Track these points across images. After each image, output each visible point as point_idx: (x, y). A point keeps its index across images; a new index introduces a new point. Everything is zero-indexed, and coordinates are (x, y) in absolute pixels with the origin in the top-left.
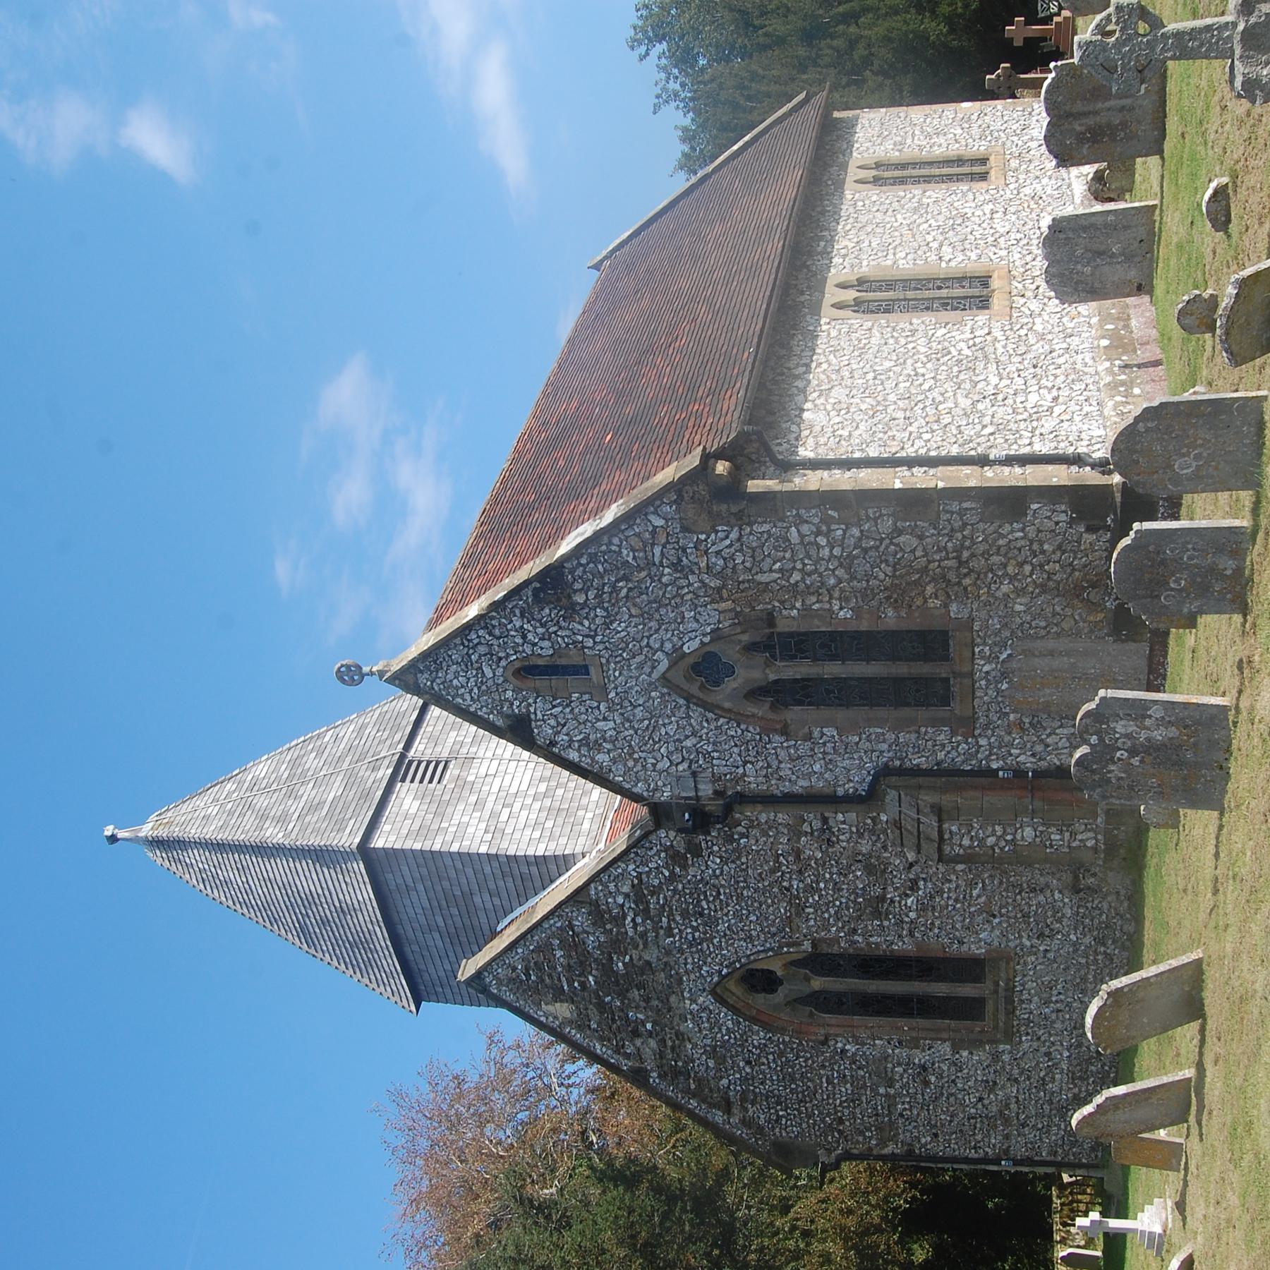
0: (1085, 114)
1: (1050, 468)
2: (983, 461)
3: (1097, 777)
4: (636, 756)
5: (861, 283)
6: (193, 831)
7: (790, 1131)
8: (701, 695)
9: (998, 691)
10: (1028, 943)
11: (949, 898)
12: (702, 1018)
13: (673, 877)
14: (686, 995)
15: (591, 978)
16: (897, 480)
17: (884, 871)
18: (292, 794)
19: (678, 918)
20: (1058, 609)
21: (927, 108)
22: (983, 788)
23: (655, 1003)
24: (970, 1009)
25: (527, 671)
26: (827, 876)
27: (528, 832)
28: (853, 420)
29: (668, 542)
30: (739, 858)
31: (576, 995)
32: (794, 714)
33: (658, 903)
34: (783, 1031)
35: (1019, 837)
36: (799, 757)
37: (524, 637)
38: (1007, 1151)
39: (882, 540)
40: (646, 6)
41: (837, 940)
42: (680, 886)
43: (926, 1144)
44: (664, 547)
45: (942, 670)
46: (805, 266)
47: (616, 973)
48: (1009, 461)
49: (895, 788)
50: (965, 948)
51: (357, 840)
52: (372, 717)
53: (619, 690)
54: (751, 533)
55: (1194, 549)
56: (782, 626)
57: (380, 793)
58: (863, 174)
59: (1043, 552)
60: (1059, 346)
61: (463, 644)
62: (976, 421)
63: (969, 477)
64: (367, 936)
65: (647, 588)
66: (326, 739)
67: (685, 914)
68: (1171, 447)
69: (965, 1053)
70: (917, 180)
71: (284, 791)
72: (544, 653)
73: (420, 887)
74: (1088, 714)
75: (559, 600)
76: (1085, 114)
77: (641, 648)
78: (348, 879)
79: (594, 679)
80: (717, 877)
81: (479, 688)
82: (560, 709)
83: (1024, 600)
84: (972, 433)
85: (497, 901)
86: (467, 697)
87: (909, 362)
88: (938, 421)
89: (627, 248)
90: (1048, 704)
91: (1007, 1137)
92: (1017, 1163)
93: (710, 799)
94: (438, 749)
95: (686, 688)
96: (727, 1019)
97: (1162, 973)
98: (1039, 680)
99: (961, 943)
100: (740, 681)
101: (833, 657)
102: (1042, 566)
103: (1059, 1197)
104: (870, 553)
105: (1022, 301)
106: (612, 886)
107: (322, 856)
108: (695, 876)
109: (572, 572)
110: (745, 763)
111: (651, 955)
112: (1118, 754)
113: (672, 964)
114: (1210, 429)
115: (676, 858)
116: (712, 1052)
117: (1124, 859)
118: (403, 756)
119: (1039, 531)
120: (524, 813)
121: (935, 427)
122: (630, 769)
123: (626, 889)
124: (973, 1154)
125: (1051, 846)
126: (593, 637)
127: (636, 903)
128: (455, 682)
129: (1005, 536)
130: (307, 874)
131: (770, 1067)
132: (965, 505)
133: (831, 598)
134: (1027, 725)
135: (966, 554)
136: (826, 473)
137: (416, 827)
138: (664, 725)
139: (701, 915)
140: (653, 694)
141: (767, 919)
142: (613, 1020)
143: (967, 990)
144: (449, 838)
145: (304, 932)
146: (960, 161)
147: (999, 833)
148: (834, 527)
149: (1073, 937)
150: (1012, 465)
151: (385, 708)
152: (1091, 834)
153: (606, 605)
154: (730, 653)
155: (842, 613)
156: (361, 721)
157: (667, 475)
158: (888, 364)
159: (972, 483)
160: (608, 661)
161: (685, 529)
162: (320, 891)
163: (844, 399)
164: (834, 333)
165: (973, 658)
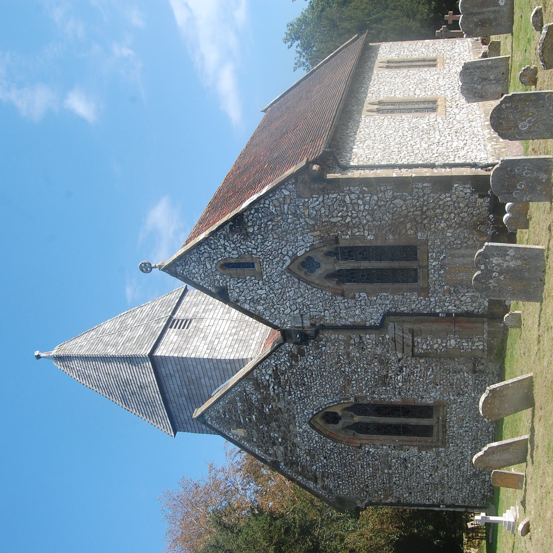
0: (479, 14)
1: (463, 169)
2: (433, 166)
3: (484, 286)
4: (275, 307)
5: (380, 103)
7: (344, 492)
8: (305, 277)
9: (440, 275)
10: (452, 398)
11: (417, 376)
12: (305, 436)
13: (292, 366)
14: (297, 424)
15: (254, 416)
16: (395, 173)
17: (388, 363)
18: (120, 335)
19: (294, 386)
20: (466, 235)
21: (410, 42)
22: (433, 322)
23: (283, 428)
24: (426, 431)
25: (227, 265)
26: (362, 365)
27: (226, 349)
28: (375, 152)
29: (291, 203)
30: (321, 357)
32: (347, 286)
33: (285, 379)
34: (341, 442)
35: (448, 344)
36: (349, 307)
37: (225, 249)
38: (443, 501)
39: (387, 201)
40: (291, 25)
41: (366, 397)
42: (295, 370)
43: (406, 497)
44: (289, 205)
45: (413, 265)
46: (355, 97)
47: (265, 414)
48: (444, 166)
49: (393, 322)
50: (424, 400)
51: (149, 352)
53: (268, 274)
54: (328, 198)
55: (528, 169)
56: (342, 244)
57: (160, 332)
58: (381, 65)
59: (460, 207)
60: (467, 125)
61: (197, 252)
62: (430, 152)
63: (427, 172)
65: (281, 225)
67: (297, 384)
68: (517, 117)
69: (424, 453)
70: (405, 67)
71: (117, 334)
72: (234, 256)
73: (177, 375)
74: (480, 254)
75: (241, 231)
76: (479, 14)
77: (278, 254)
78: (144, 371)
79: (257, 269)
80: (312, 366)
81: (204, 274)
82: (241, 284)
83: (451, 231)
84: (428, 156)
85: (212, 382)
86: (199, 278)
87: (400, 131)
88: (413, 152)
89: (278, 102)
90: (462, 281)
91: (443, 494)
92: (447, 506)
93: (309, 328)
94: (187, 315)
95: (298, 274)
96: (316, 436)
97: (514, 382)
98: (458, 269)
99: (422, 398)
100: (323, 270)
101: (365, 259)
102: (459, 214)
103: (466, 538)
104: (382, 208)
105: (451, 109)
106: (264, 371)
107: (132, 360)
108: (301, 366)
109: (247, 217)
110: (325, 310)
111: (281, 405)
112: (494, 274)
113: (291, 409)
114: (535, 108)
115: (293, 357)
116: (309, 453)
117: (496, 355)
118: (171, 317)
119: (458, 197)
120: (225, 342)
121: (412, 154)
123: (270, 372)
124: (427, 503)
125: (463, 349)
126: (256, 249)
127: (274, 379)
128: (193, 271)
129: (442, 200)
130: (126, 370)
131: (335, 460)
132: (425, 185)
133: (364, 230)
134: (452, 291)
135: (425, 208)
136: (362, 171)
137: (175, 347)
138: (288, 292)
139: (304, 385)
140: (283, 276)
141: (334, 386)
142: (264, 437)
143: (425, 422)
144: (190, 352)
145: (124, 399)
146: (424, 60)
147: (439, 343)
148: (366, 195)
149: (473, 395)
150: (446, 168)
151: (164, 298)
152: (481, 343)
153: (262, 233)
154: (318, 256)
155: (369, 237)
156: (153, 304)
157: (292, 170)
158: (391, 132)
159: (428, 175)
160: (263, 260)
161: (299, 196)
162: (131, 378)
163: (371, 144)
164: (367, 121)
165: (428, 259)
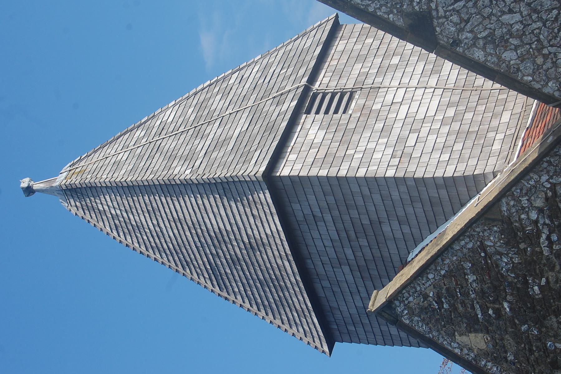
4: (545, 51)
6: (104, 177)
15: (506, 305)
18: (199, 133)
27: (436, 155)
31: (491, 324)
47: (532, 298)
51: (263, 169)
52: (275, 59)
57: (284, 124)
64: (277, 272)
66: (232, 81)
71: (191, 132)
73: (328, 217)
78: (255, 212)
94: (343, 81)
107: (229, 189)
118: (307, 89)
120: (432, 138)
122: (539, 67)
123: (539, 203)
130: (215, 210)
137: (321, 155)
142: (531, 351)
144: (355, 164)
151: (289, 47)
162: (229, 228)
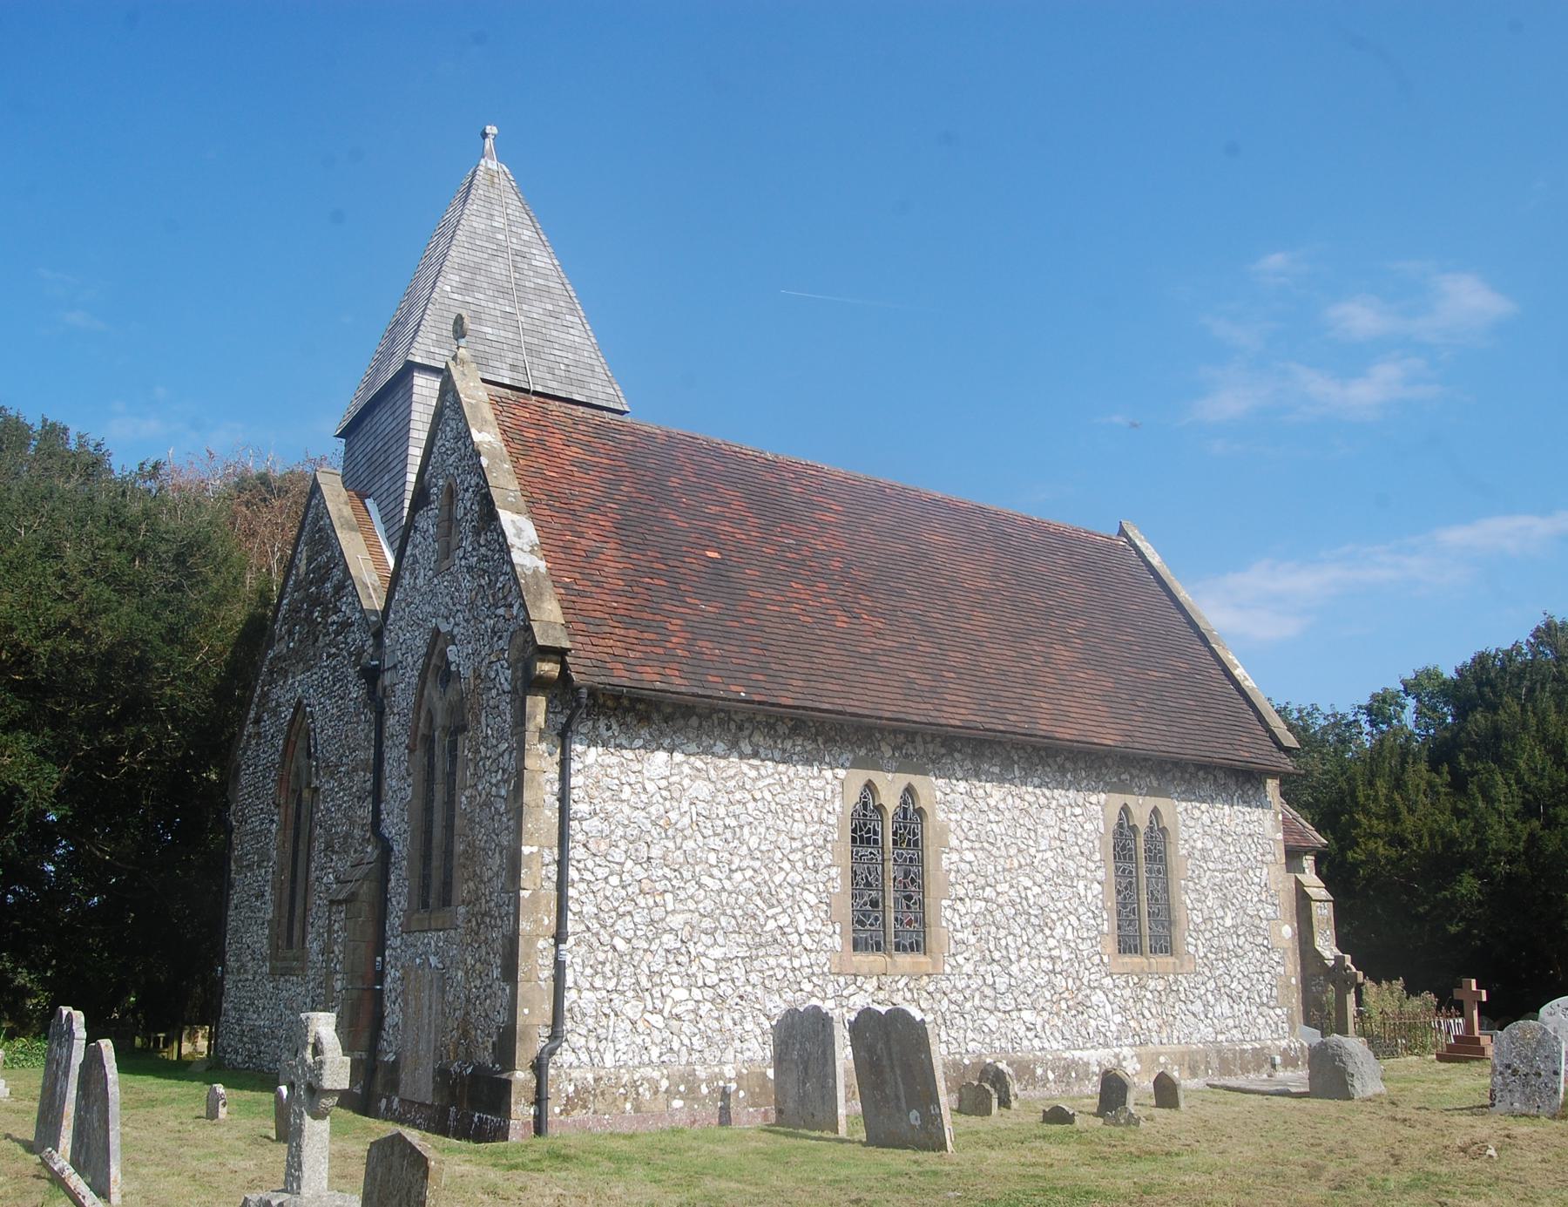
51: (418, 360)
